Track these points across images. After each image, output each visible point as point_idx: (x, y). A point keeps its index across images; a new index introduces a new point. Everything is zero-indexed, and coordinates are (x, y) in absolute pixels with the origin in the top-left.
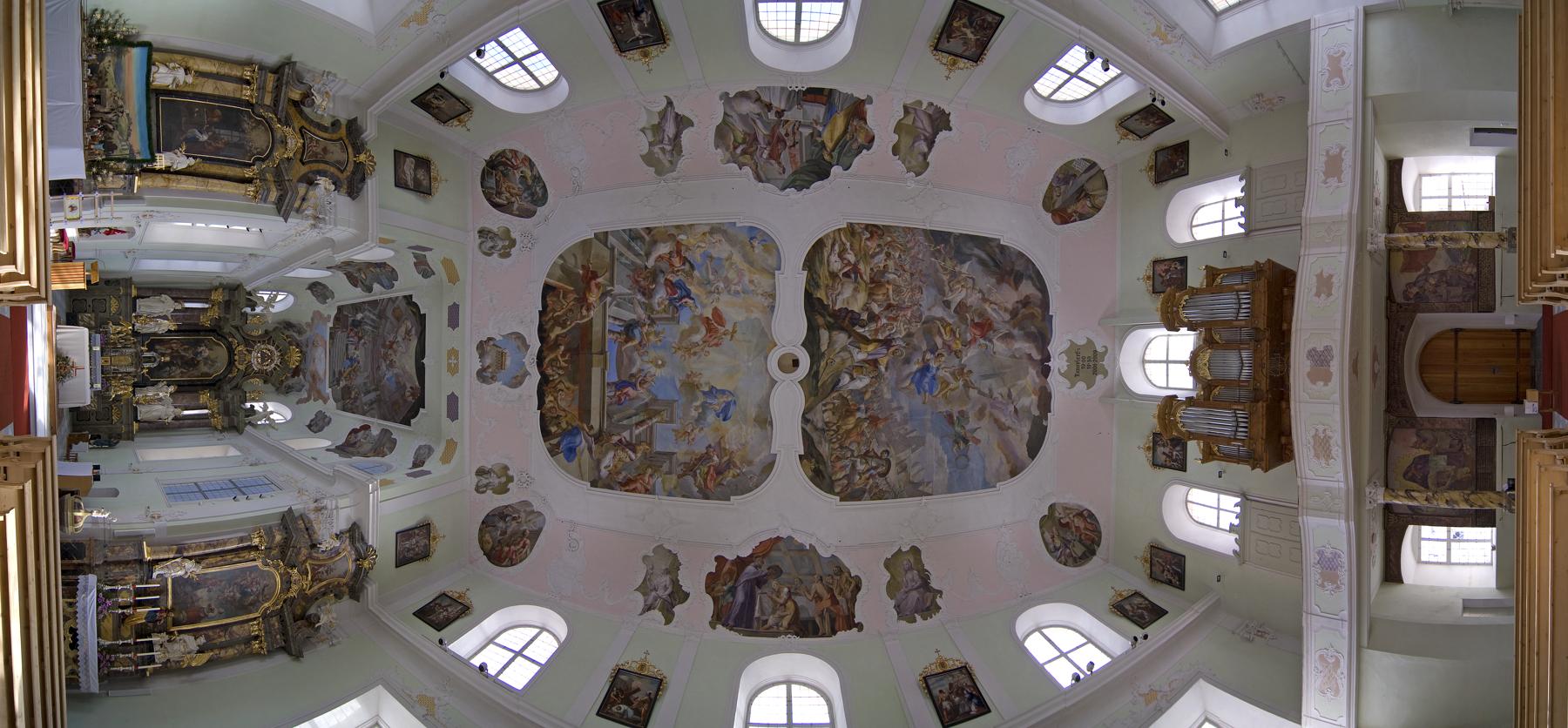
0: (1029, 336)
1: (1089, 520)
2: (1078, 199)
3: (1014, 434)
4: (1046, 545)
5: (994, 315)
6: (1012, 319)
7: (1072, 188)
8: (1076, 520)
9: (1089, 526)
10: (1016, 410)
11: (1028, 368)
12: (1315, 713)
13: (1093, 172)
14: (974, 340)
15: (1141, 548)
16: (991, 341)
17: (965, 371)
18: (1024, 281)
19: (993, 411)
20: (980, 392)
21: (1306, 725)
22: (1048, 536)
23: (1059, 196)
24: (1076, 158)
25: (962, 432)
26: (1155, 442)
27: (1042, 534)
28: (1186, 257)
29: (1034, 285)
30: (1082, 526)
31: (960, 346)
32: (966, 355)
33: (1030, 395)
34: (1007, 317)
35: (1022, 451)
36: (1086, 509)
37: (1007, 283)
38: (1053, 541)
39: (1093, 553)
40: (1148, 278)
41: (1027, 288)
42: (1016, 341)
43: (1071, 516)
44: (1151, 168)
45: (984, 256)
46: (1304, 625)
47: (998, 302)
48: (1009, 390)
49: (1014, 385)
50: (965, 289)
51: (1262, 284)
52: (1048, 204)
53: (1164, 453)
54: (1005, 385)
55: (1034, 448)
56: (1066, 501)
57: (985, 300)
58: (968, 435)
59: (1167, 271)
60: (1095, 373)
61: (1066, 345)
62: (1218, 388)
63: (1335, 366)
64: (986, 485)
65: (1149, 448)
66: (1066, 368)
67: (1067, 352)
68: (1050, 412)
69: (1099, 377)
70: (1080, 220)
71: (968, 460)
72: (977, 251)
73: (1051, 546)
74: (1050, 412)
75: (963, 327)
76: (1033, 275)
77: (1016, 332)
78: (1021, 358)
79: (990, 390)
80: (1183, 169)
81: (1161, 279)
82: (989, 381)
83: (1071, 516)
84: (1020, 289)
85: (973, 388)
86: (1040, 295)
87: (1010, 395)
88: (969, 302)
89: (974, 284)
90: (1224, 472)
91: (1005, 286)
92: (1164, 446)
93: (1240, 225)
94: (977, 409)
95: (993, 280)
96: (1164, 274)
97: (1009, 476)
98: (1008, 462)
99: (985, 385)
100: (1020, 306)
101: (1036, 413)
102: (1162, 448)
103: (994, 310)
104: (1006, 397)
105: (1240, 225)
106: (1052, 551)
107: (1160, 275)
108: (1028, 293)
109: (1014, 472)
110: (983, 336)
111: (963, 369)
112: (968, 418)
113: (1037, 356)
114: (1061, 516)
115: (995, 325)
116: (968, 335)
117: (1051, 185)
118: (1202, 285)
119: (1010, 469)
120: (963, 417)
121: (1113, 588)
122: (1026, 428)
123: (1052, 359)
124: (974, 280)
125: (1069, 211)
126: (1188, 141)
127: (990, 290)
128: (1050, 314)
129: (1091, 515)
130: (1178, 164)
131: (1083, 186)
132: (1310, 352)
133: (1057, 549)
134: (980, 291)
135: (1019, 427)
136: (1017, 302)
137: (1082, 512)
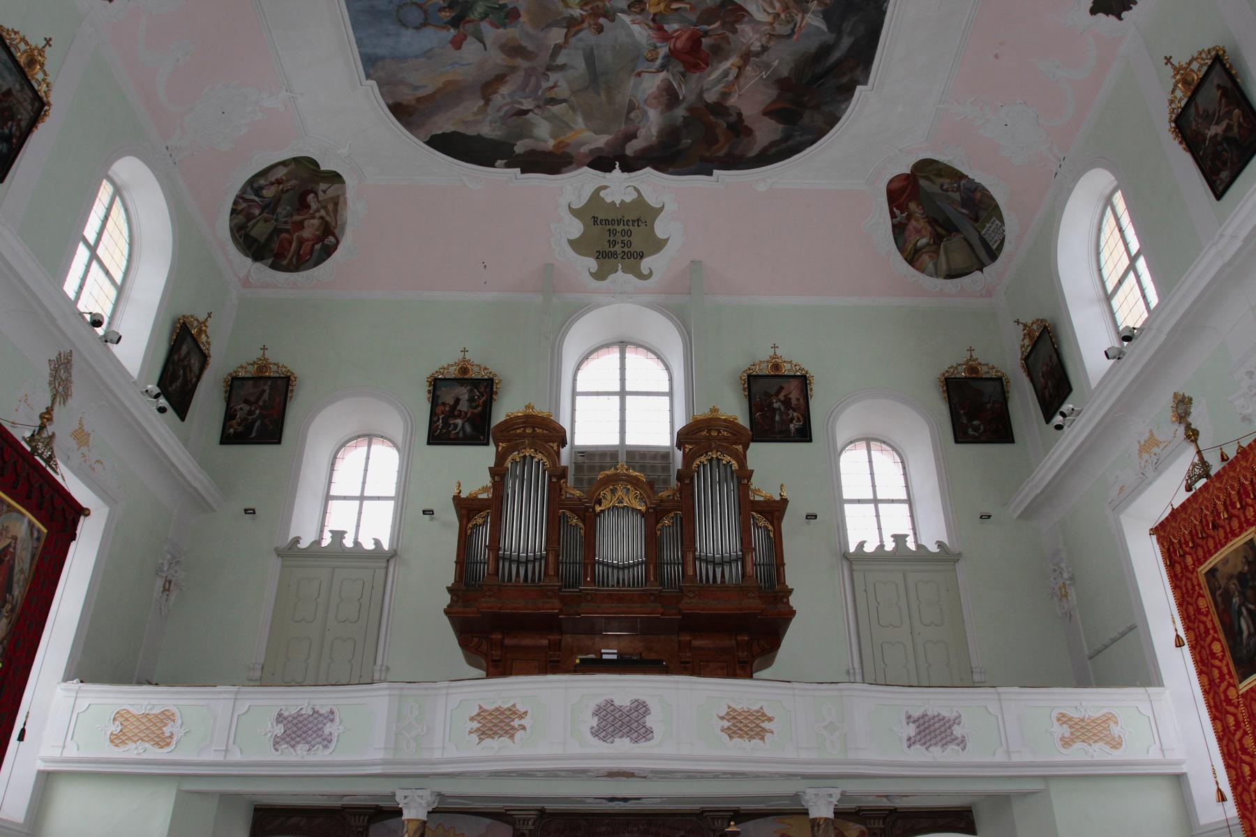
0: (670, 135)
1: (318, 247)
2: (932, 221)
3: (475, 109)
4: (264, 173)
5: (715, 75)
6: (707, 105)
7: (956, 213)
8: (316, 222)
9: (306, 248)
10: (526, 112)
11: (609, 134)
12: (83, 704)
13: (983, 254)
14: (665, 37)
15: (284, 357)
16: (663, 68)
17: (602, 21)
18: (781, 127)
19: (522, 73)
20: (558, 49)
21: (67, 690)
22: (281, 173)
23: (941, 187)
24: (1006, 228)
25: (475, 15)
26: (475, 383)
27: (284, 163)
28: (810, 441)
29: (773, 144)
30: (307, 233)
31: (653, 10)
32: (634, 22)
33: (554, 136)
34: (711, 97)
35: (444, 124)
36: (338, 242)
37: (779, 96)
38: (272, 184)
39: (257, 257)
40: (776, 367)
41: (766, 132)
42: (662, 113)
43: (323, 213)
44: (973, 369)
45: (836, 55)
46: (218, 689)
47: (742, 81)
48: (565, 101)
49: (573, 108)
50: (769, 19)
51: (753, 603)
52: (926, 168)
53: (457, 401)
54: (574, 93)
55: (447, 144)
56: (349, 202)
57: (747, 57)
58: (469, 27)
59: (787, 402)
60: (601, 255)
61: (652, 200)
62: (581, 525)
63: (622, 745)
64: (371, 63)
65: (464, 370)
66: (608, 200)
67: (640, 202)
68: (523, 172)
69: (592, 264)
70: (894, 226)
71: (417, 28)
72: (846, 42)
73: (262, 182)
74: (523, 172)
75: (693, 17)
76: (790, 142)
77: (680, 112)
78: (628, 119)
79: (562, 68)
80: (966, 433)
81: (773, 390)
82: (581, 65)
83: (323, 213)
84: (766, 119)
85: (566, 35)
86: (752, 154)
87: (553, 101)
88: (745, 28)
89: (780, 37)
90: (432, 520)
91: (773, 93)
92: (471, 400)
93: (861, 545)
94: (524, 43)
95: (785, 73)
96: (781, 397)
97: (391, 102)
98: (419, 100)
99: (574, 59)
100: (733, 119)
101: (520, 148)
102: (466, 397)
103: (726, 74)
104: (549, 95)
105: (861, 545)
106: (254, 184)
107: (781, 388)
108: (757, 133)
109: (398, 110)
110: (673, 54)
111: (605, 16)
112: (504, 26)
113: (632, 148)
114: (320, 193)
115: (695, 76)
116: (676, 26)
117: (962, 176)
118: (757, 491)
119: (405, 103)
120: (506, 17)
121: (209, 315)
122: (488, 129)
123: (626, 175)
124: (789, 36)
125: (913, 206)
126: (1013, 442)
127: (767, 66)
128: (716, 172)
129: (328, 251)
130: (976, 423)
131: (957, 231)
132: (644, 705)
133: (257, 192)
134: (765, 49)
135: (489, 118)
136: (740, 115)
137: (333, 235)
